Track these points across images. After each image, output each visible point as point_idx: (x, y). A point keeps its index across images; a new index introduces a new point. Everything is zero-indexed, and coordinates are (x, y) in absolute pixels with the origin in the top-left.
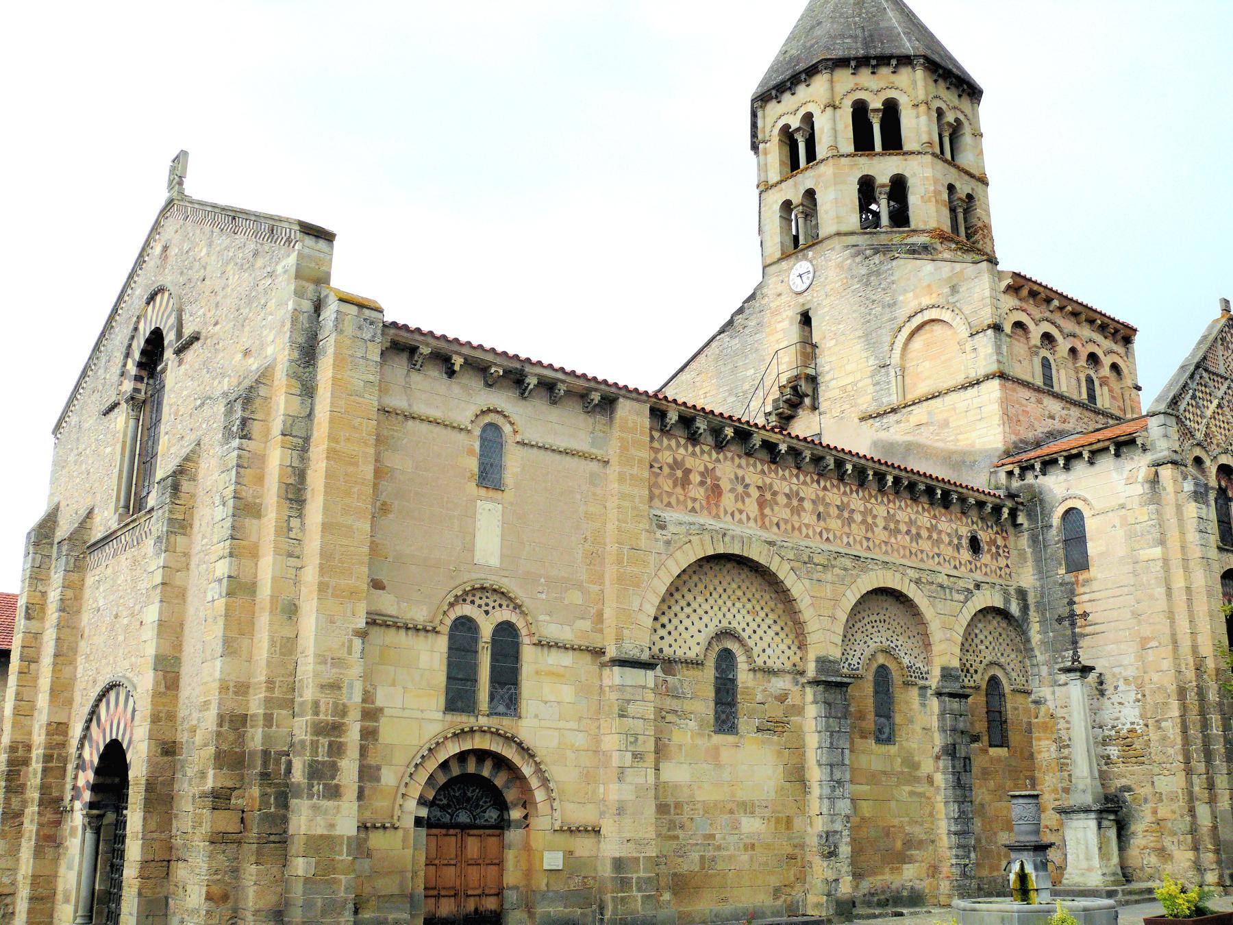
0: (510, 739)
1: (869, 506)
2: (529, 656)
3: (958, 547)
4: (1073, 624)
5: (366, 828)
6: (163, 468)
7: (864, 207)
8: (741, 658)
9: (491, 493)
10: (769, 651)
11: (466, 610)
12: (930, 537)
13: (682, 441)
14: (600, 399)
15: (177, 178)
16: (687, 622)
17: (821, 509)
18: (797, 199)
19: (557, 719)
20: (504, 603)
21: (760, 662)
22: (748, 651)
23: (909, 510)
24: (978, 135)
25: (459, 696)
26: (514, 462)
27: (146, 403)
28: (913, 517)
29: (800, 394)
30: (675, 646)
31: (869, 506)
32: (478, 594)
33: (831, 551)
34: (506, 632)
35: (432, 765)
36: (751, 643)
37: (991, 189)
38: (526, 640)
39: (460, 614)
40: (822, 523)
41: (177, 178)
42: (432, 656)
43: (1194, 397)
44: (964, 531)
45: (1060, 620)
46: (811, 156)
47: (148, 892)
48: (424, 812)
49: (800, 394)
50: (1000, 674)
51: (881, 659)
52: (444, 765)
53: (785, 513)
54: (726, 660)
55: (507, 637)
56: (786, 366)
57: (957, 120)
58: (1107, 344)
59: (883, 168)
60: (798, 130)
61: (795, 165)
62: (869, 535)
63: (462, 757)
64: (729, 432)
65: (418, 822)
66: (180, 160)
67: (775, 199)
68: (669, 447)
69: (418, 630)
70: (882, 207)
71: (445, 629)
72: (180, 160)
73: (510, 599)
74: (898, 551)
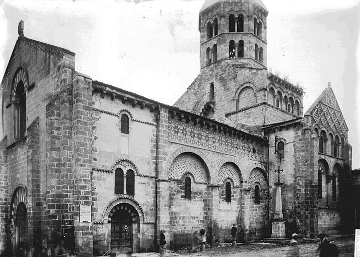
0: (133, 201)
1: (200, 132)
2: (137, 180)
3: (249, 152)
4: (279, 173)
5: (95, 224)
6: (28, 124)
7: (231, 50)
8: (192, 180)
9: (125, 134)
10: (199, 178)
11: (120, 166)
12: (183, 133)
13: (177, 121)
14: (154, 107)
15: (20, 31)
16: (178, 170)
17: (176, 130)
18: (211, 47)
19: (143, 195)
20: (130, 164)
21: (196, 181)
22: (194, 178)
23: (183, 125)
24: (265, 28)
25: (118, 190)
26: (132, 125)
27: (20, 104)
28: (185, 128)
29: (209, 108)
30: (175, 176)
31: (200, 132)
32: (123, 162)
33: (216, 153)
34: (130, 172)
35: (111, 207)
36: (194, 176)
37: (267, 45)
38: (136, 174)
39: (120, 167)
40: (214, 144)
41: (20, 31)
42: (111, 179)
43: (317, 111)
44: (252, 147)
45: (276, 171)
46: (216, 34)
47: (351, 242)
48: (110, 219)
49: (209, 108)
50: (259, 185)
51: (228, 180)
52: (115, 208)
53: (204, 141)
54: (188, 180)
55: (131, 174)
56: (206, 99)
57: (260, 22)
58: (296, 95)
59: (237, 39)
60: (212, 24)
61: (211, 36)
62: (200, 141)
63: (119, 205)
64: (175, 113)
65: (109, 222)
66: (21, 24)
67: (206, 47)
68: (173, 122)
69: (98, 171)
70: (236, 51)
71: (114, 172)
72: (21, 24)
73: (131, 163)
74: (208, 146)
